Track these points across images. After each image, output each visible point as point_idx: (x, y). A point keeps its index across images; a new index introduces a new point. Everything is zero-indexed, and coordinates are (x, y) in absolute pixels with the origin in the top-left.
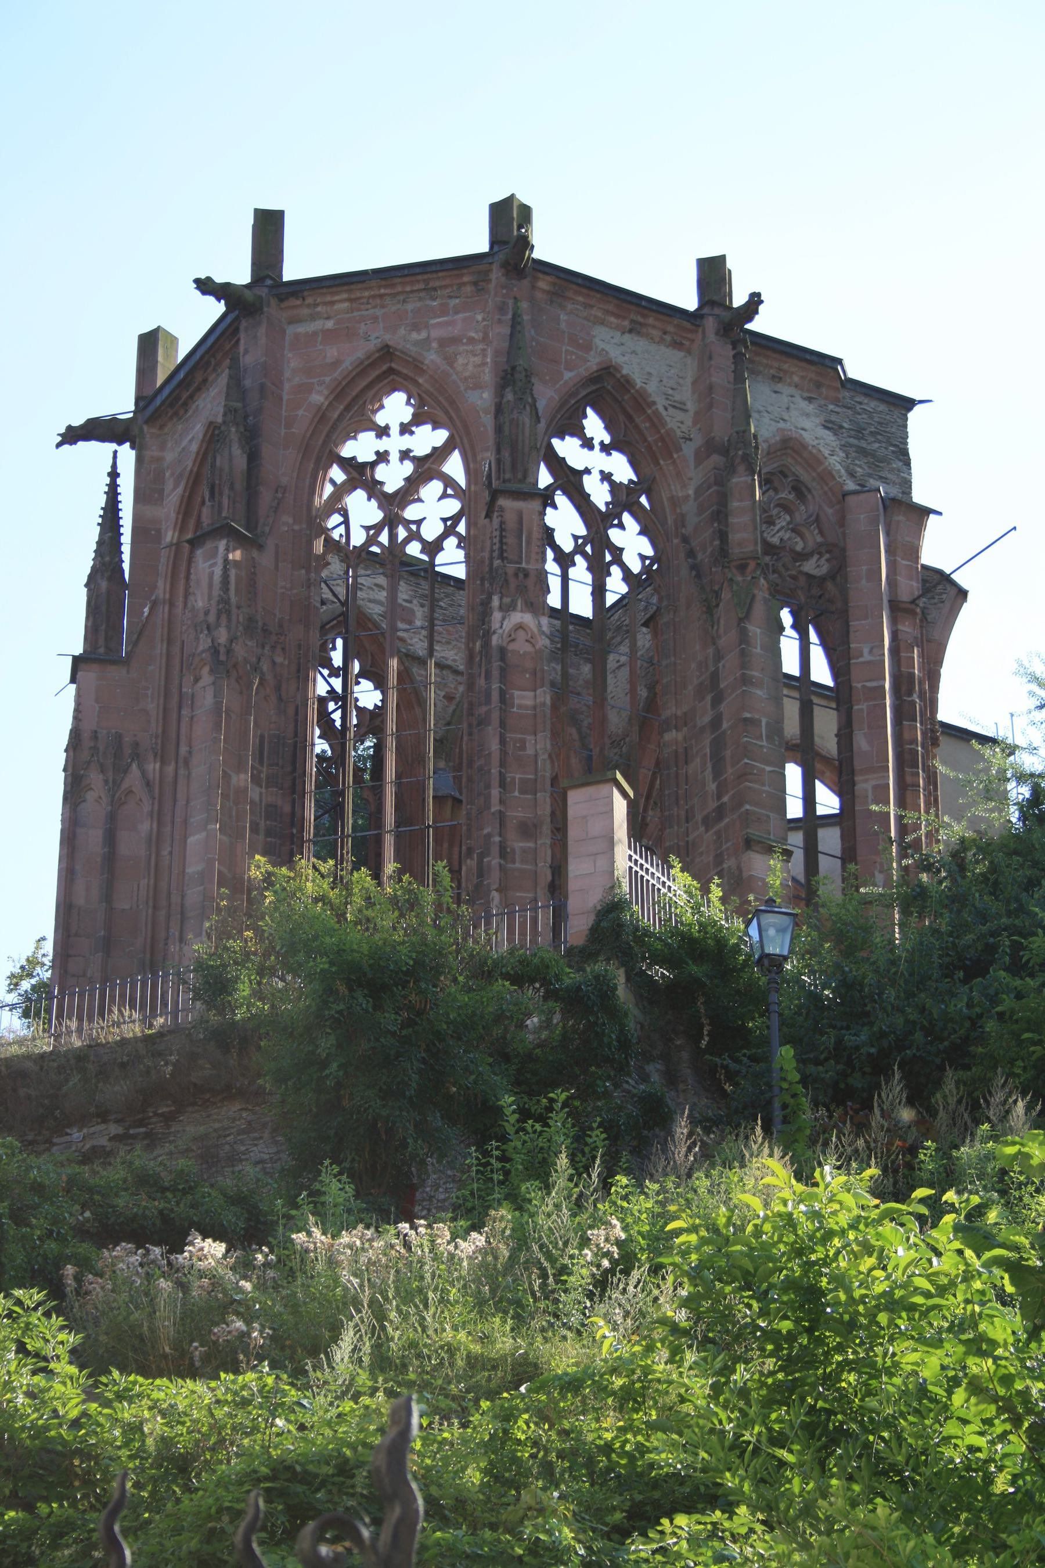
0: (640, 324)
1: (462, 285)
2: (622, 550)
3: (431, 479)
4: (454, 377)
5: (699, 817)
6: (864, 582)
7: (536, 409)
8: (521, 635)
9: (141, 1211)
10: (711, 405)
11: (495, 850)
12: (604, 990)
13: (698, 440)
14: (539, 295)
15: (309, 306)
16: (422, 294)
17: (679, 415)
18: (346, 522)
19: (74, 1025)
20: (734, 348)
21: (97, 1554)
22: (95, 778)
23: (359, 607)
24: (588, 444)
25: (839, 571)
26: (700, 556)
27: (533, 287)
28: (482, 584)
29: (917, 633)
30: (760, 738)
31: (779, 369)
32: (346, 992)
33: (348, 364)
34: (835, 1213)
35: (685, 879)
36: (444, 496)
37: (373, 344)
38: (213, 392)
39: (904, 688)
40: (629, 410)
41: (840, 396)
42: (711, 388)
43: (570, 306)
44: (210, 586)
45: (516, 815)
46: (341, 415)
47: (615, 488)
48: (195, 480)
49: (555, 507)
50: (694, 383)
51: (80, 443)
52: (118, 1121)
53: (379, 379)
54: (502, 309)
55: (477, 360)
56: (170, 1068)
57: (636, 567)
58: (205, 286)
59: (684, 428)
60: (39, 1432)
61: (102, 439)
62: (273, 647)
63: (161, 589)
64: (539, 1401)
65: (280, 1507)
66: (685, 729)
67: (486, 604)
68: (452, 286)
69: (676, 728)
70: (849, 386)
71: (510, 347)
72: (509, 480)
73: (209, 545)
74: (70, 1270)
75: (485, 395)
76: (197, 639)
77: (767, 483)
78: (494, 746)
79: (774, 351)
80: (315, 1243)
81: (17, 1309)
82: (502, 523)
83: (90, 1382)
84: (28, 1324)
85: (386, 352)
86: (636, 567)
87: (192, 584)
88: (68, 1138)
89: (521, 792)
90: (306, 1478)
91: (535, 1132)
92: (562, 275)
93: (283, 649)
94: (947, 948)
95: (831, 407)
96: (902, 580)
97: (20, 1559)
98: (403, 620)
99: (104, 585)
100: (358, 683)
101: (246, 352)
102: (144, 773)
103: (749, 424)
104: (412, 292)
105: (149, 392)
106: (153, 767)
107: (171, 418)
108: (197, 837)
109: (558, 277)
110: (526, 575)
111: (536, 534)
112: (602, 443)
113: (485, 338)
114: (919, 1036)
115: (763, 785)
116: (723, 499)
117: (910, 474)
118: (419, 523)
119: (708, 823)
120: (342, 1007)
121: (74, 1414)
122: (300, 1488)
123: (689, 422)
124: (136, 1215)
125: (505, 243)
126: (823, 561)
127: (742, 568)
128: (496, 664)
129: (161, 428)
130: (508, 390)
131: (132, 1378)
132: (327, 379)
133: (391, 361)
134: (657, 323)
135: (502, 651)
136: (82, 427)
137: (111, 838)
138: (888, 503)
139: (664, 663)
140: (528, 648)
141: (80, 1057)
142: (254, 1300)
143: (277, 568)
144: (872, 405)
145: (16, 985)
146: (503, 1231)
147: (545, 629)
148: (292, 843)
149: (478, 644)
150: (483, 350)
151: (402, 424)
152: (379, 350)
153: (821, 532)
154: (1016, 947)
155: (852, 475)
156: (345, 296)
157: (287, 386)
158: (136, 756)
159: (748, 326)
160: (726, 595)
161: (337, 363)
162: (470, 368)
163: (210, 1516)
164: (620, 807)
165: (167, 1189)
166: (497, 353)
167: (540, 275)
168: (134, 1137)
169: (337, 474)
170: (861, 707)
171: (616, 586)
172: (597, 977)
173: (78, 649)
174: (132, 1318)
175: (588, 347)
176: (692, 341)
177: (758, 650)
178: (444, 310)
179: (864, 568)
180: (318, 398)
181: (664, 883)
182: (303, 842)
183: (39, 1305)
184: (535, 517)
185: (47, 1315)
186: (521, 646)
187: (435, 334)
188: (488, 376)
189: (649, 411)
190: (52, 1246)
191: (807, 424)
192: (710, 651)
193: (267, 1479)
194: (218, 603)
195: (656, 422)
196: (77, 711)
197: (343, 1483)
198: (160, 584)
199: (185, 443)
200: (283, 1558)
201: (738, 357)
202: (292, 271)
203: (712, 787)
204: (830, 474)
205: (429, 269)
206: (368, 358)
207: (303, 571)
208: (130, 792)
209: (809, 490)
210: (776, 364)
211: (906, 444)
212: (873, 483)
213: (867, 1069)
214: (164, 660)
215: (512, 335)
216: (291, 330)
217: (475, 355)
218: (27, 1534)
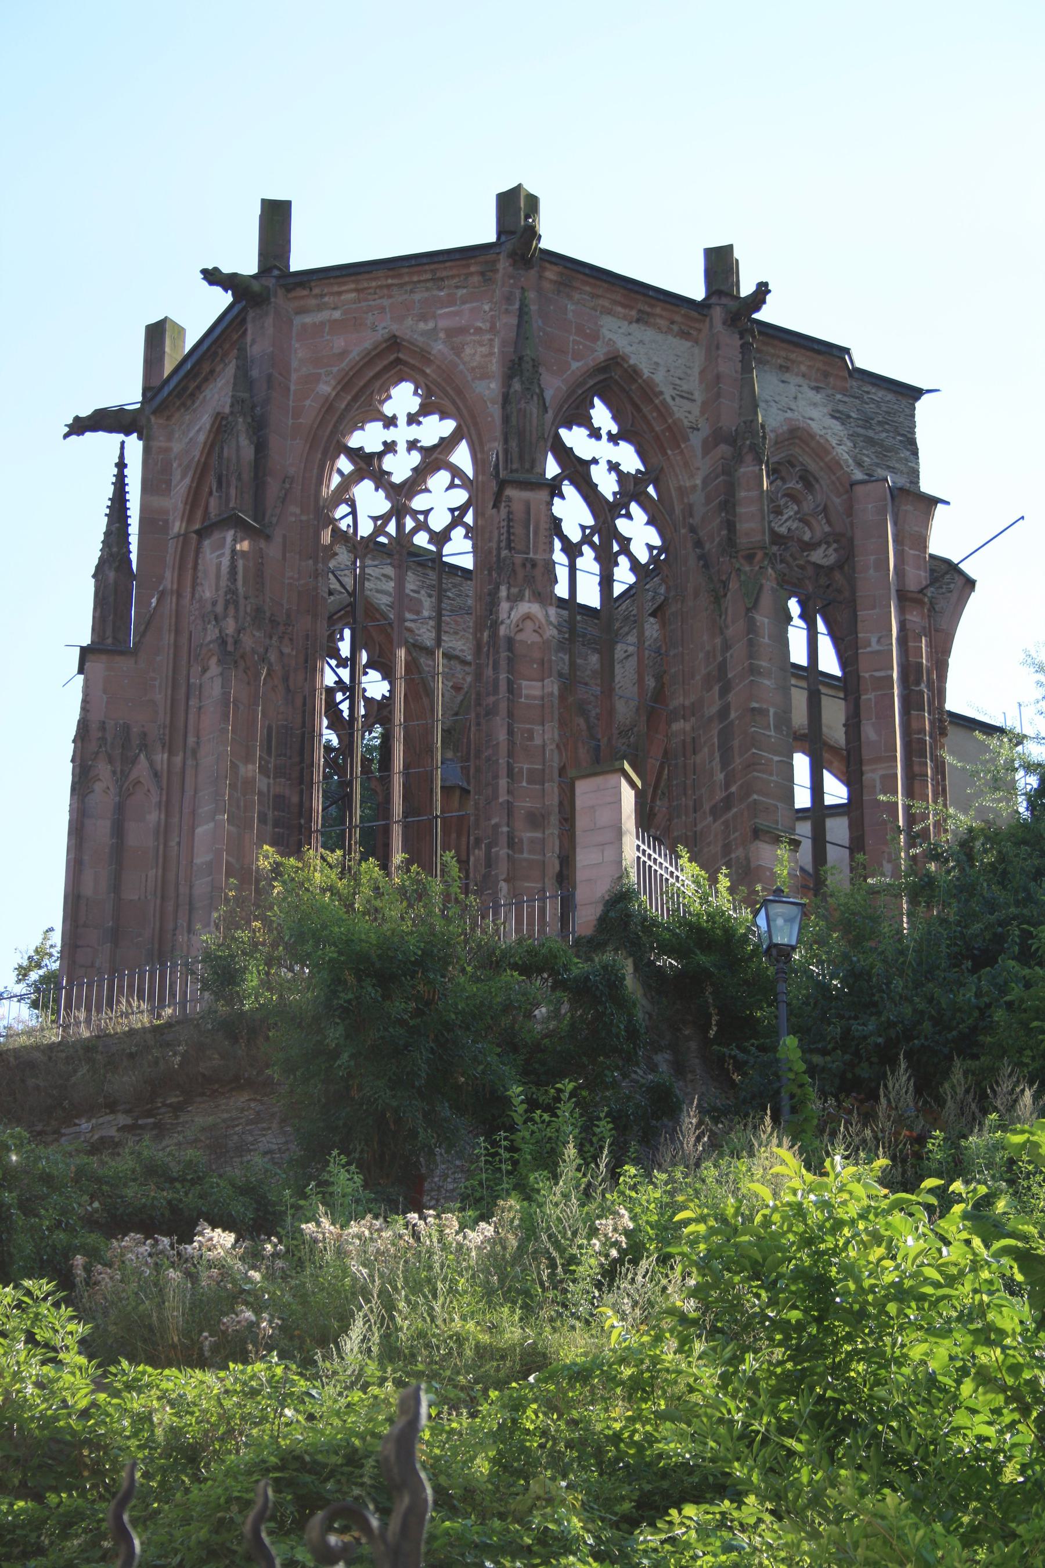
0: (648, 314)
2: (629, 540)
3: (439, 469)
4: (461, 367)
5: (707, 807)
6: (871, 571)
7: (544, 399)
10: (718, 395)
11: (503, 840)
12: (612, 980)
13: (705, 430)
14: (546, 285)
15: (316, 296)
17: (687, 405)
18: (354, 513)
19: (82, 1016)
20: (741, 338)
21: (106, 1544)
22: (103, 769)
24: (595, 434)
25: (847, 560)
26: (707, 546)
27: (541, 277)
28: (490, 574)
30: (768, 727)
31: (787, 359)
33: (355, 354)
34: (844, 1203)
36: (452, 486)
37: (381, 334)
38: (220, 383)
39: (912, 678)
40: (636, 399)
41: (848, 386)
42: (718, 378)
43: (577, 296)
44: (218, 576)
45: (525, 804)
46: (348, 404)
47: (623, 478)
48: (202, 471)
49: (563, 497)
51: (88, 434)
52: (127, 1112)
54: (509, 299)
55: (484, 350)
56: (178, 1058)
57: (643, 557)
58: (212, 276)
59: (692, 418)
61: (110, 430)
62: (281, 638)
64: (548, 1391)
65: (289, 1497)
66: (693, 719)
68: (459, 276)
70: (856, 375)
71: (518, 335)
72: (516, 471)
73: (217, 535)
74: (79, 1260)
75: (493, 385)
76: (205, 629)
77: (774, 472)
78: (502, 736)
79: (783, 341)
80: (324, 1234)
81: (26, 1299)
82: (509, 513)
83: (100, 1372)
84: (37, 1314)
85: (394, 343)
86: (643, 557)
87: (200, 574)
88: (77, 1129)
89: (528, 783)
90: (315, 1468)
91: (543, 1122)
92: (569, 265)
93: (291, 640)
95: (839, 397)
97: (29, 1549)
98: (410, 611)
99: (112, 575)
100: (366, 674)
101: (254, 341)
102: (151, 763)
103: (756, 414)
104: (419, 282)
105: (156, 383)
106: (161, 758)
107: (178, 409)
108: (206, 827)
110: (534, 565)
111: (544, 525)
112: (609, 433)
113: (492, 329)
114: (927, 1026)
115: (771, 774)
116: (731, 488)
117: (918, 463)
118: (426, 513)
119: (715, 812)
120: (350, 996)
121: (83, 1404)
122: (308, 1478)
123: (696, 410)
124: (144, 1206)
125: (513, 233)
126: (831, 551)
127: (750, 558)
128: (504, 654)
129: (169, 418)
130: (516, 380)
131: (140, 1368)
132: (335, 369)
133: (399, 351)
134: (664, 313)
135: (510, 641)
136: (89, 417)
137: (119, 830)
138: (895, 492)
139: (672, 653)
140: (536, 638)
141: (88, 1048)
142: (263, 1290)
143: (284, 558)
144: (879, 394)
145: (25, 975)
146: (512, 1221)
147: (553, 619)
148: (300, 833)
149: (486, 634)
150: (491, 340)
151: (409, 415)
152: (386, 341)
153: (829, 522)
154: (1027, 935)
155: (859, 464)
156: (352, 286)
157: (294, 377)
158: (144, 746)
159: (755, 316)
160: (733, 585)
161: (344, 353)
162: (477, 358)
163: (219, 1505)
164: (628, 797)
167: (547, 265)
168: (142, 1127)
169: (344, 464)
170: (869, 697)
171: (624, 576)
172: (605, 967)
173: (86, 640)
174: (141, 1308)
175: (595, 337)
177: (766, 640)
178: (451, 301)
179: (872, 558)
180: (325, 388)
181: (672, 873)
184: (543, 507)
185: (56, 1305)
186: (528, 636)
187: (443, 323)
188: (495, 366)
189: (657, 401)
190: (61, 1236)
191: (815, 413)
192: (718, 641)
193: (276, 1468)
194: (226, 594)
195: (664, 412)
196: (85, 702)
198: (168, 574)
199: (192, 434)
200: (292, 1548)
201: (745, 347)
202: (298, 262)
203: (720, 777)
204: (838, 463)
205: (436, 259)
206: (375, 348)
207: (311, 562)
208: (138, 783)
209: (817, 481)
210: (783, 354)
211: (914, 433)
212: (880, 472)
213: (875, 1060)
214: (172, 651)
215: (519, 326)
216: (298, 321)
217: (482, 345)
218: (37, 1524)
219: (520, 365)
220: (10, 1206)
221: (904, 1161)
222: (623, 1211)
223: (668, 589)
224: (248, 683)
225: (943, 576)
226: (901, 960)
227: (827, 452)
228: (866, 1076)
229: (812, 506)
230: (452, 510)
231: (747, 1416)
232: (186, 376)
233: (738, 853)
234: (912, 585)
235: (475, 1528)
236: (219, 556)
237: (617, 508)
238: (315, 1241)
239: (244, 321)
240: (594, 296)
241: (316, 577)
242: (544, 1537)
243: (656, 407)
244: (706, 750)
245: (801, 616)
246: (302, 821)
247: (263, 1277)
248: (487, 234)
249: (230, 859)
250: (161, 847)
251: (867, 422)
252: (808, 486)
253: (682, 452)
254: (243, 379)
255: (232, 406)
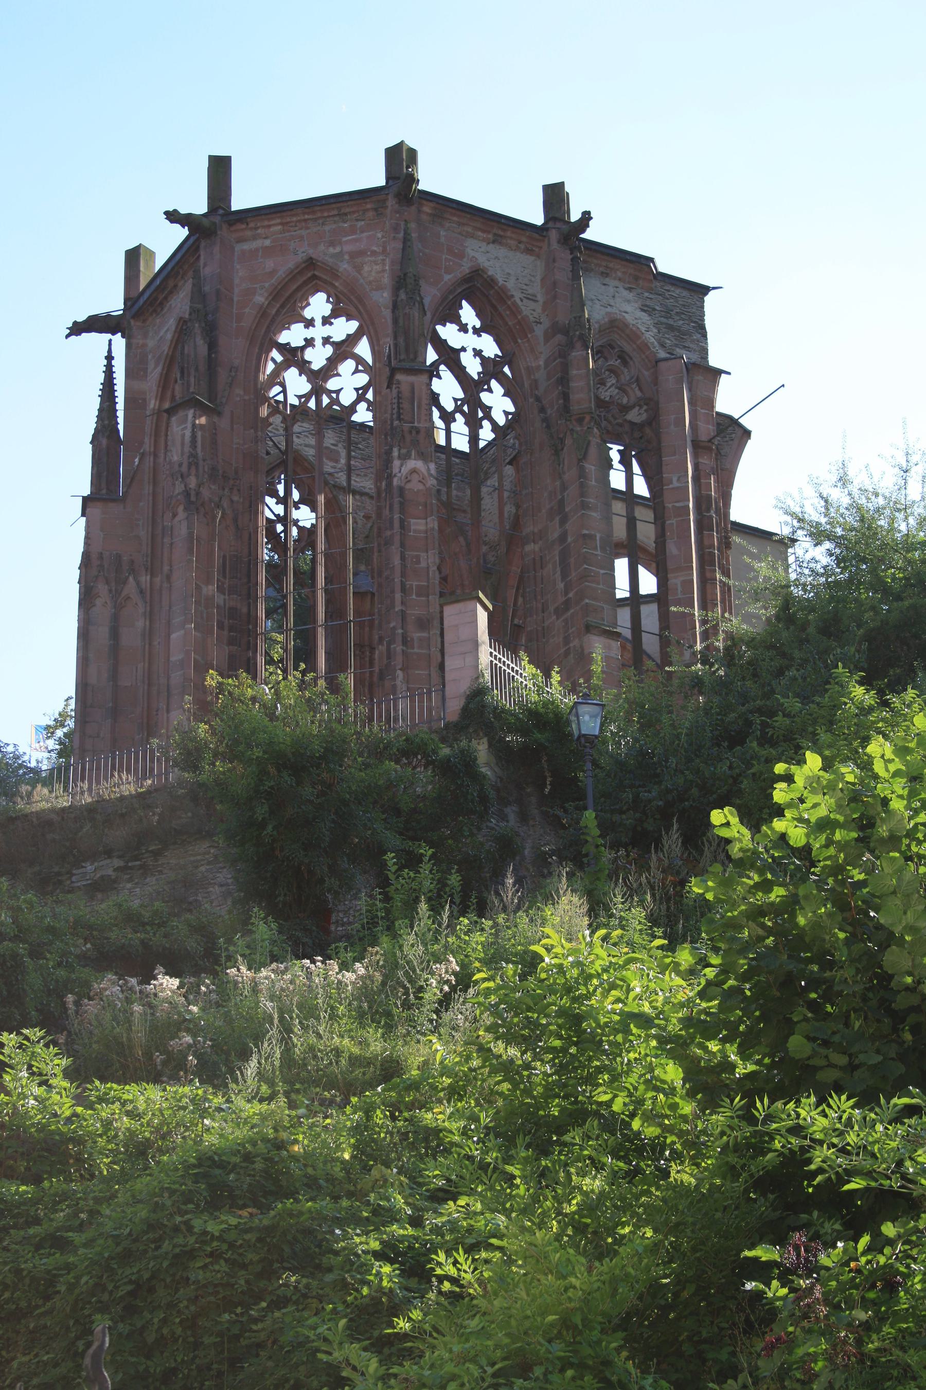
0: (501, 236)
1: (365, 211)
2: (490, 408)
3: (347, 358)
4: (362, 281)
5: (552, 609)
6: (672, 427)
7: (423, 305)
8: (415, 477)
9: (127, 942)
10: (555, 297)
11: (399, 639)
12: (468, 762)
13: (546, 323)
14: (424, 217)
15: (251, 229)
16: (336, 219)
17: (532, 305)
18: (284, 391)
19: (86, 786)
20: (571, 254)
21: (82, 1215)
22: (102, 588)
23: (297, 451)
24: (463, 328)
25: (654, 420)
26: (549, 411)
27: (419, 211)
28: (386, 438)
29: (712, 463)
30: (596, 548)
31: (607, 267)
32: (276, 773)
33: (281, 273)
34: (592, 962)
35: (530, 669)
36: (356, 371)
37: (301, 257)
38: (182, 295)
39: (704, 507)
40: (494, 302)
41: (653, 286)
42: (555, 284)
43: (447, 225)
44: (183, 444)
45: (414, 612)
46: (278, 311)
47: (485, 361)
48: (170, 361)
49: (439, 377)
50: (542, 280)
51: (84, 334)
52: (119, 857)
53: (305, 283)
54: (396, 229)
55: (379, 268)
56: (157, 818)
57: (501, 420)
58: (173, 216)
59: (535, 315)
60: (42, 1128)
62: (231, 489)
63: (148, 446)
64: (391, 1096)
65: (203, 1186)
66: (540, 542)
67: (389, 453)
68: (358, 211)
69: (534, 542)
70: (659, 278)
71: (403, 257)
72: (404, 360)
73: (181, 413)
74: (70, 998)
75: (385, 295)
76: (174, 485)
77: (599, 353)
78: (397, 561)
79: (603, 253)
80: (242, 977)
81: (25, 1042)
82: (399, 392)
83: (79, 1090)
84: (33, 1053)
85: (311, 263)
86: (501, 420)
87: (169, 443)
88: (83, 870)
89: (418, 595)
90: (222, 1165)
91: (410, 878)
92: (441, 202)
93: (239, 490)
94: (717, 725)
95: (646, 294)
96: (701, 425)
97: (30, 1219)
99: (104, 442)
100: (297, 508)
101: (205, 265)
102: (138, 583)
103: (584, 311)
104: (329, 216)
105: (134, 294)
106: (145, 579)
107: (151, 314)
108: (178, 634)
109: (438, 203)
111: (425, 400)
112: (474, 328)
113: (384, 251)
114: (695, 791)
115: (598, 584)
116: (565, 368)
117: (706, 344)
118: (338, 392)
119: (558, 612)
120: (272, 783)
121: (68, 1113)
122: (218, 1171)
123: (539, 310)
124: (124, 944)
125: (398, 178)
126: (642, 411)
127: (580, 421)
128: (397, 500)
129: (144, 321)
130: (402, 291)
131: (109, 1085)
132: (267, 285)
133: (314, 269)
134: (513, 236)
135: (401, 490)
136: (84, 322)
137: (115, 634)
138: (690, 366)
139: (524, 492)
140: (421, 487)
141: (91, 810)
142: (200, 1018)
143: (232, 429)
144: (677, 292)
145: (53, 733)
146: (378, 962)
147: (433, 472)
148: (249, 636)
149: (384, 484)
150: (383, 260)
151: (323, 318)
152: (305, 262)
153: (640, 389)
154: (764, 725)
155: (662, 345)
156: (278, 221)
157: (236, 291)
158: (133, 571)
159: (582, 236)
160: (568, 441)
161: (273, 273)
162: (373, 274)
163: (155, 1193)
164: (482, 617)
165: (147, 924)
166: (393, 263)
167: (425, 202)
168: (131, 868)
169: (275, 354)
170: (672, 522)
171: (486, 434)
172: (462, 751)
173: (87, 491)
174: (115, 1031)
175: (461, 255)
176: (541, 248)
177: (593, 483)
178: (353, 230)
180: (260, 299)
181: (517, 671)
182: (257, 635)
183: (42, 1038)
184: (424, 387)
185: (47, 1046)
186: (415, 485)
187: (347, 248)
188: (386, 280)
189: (509, 303)
190: (62, 973)
191: (629, 308)
192: (558, 483)
193: (194, 1166)
194: (189, 457)
195: (515, 311)
196: (87, 538)
197: (247, 1167)
198: (147, 440)
199: (162, 333)
200: (206, 1222)
201: (575, 260)
202: (238, 203)
203: (561, 586)
204: (646, 345)
205: (341, 199)
206: (297, 267)
207: (252, 431)
208: (128, 598)
209: (631, 359)
210: (604, 264)
211: (703, 320)
212: (678, 351)
213: (658, 816)
214: (151, 498)
215: (404, 249)
216: (238, 248)
217: (377, 264)
218: (35, 1202)
219: (405, 280)
220: (23, 956)
221: (668, 900)
222: (452, 959)
223: (520, 445)
224: (208, 524)
225: (727, 428)
226: (677, 742)
227: (638, 337)
228: (651, 829)
229: (628, 378)
230: (357, 390)
231: (482, 1153)
232: (156, 290)
233: (575, 643)
234: (703, 437)
235: (330, 1206)
236: (183, 429)
237: (481, 384)
238: (236, 983)
239: (198, 247)
240: (459, 224)
241: (257, 442)
242: (377, 1211)
243: (509, 307)
244: (550, 566)
245: (620, 462)
246: (251, 627)
247: (200, 1009)
248: (378, 179)
249: (197, 657)
250: (147, 646)
251: (668, 313)
252: (625, 363)
253: (529, 340)
254: (198, 295)
255: (190, 314)
